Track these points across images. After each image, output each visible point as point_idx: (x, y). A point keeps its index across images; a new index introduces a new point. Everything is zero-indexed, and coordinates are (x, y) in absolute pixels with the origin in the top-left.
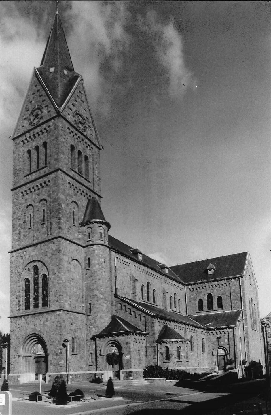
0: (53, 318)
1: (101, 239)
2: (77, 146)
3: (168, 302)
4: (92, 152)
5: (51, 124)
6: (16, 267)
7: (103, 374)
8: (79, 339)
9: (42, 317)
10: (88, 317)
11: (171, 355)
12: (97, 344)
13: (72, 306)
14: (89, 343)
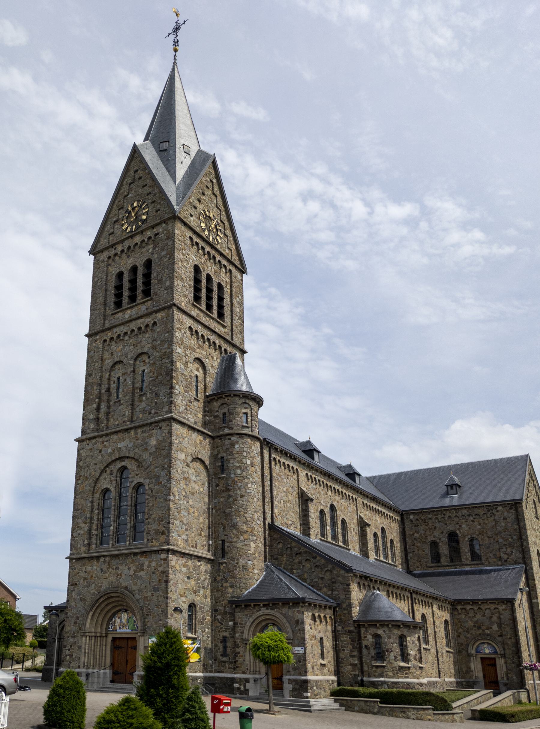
2: (206, 268)
5: (161, 230)
7: (249, 682)
9: (133, 561)
10: (219, 566)
14: (219, 617)
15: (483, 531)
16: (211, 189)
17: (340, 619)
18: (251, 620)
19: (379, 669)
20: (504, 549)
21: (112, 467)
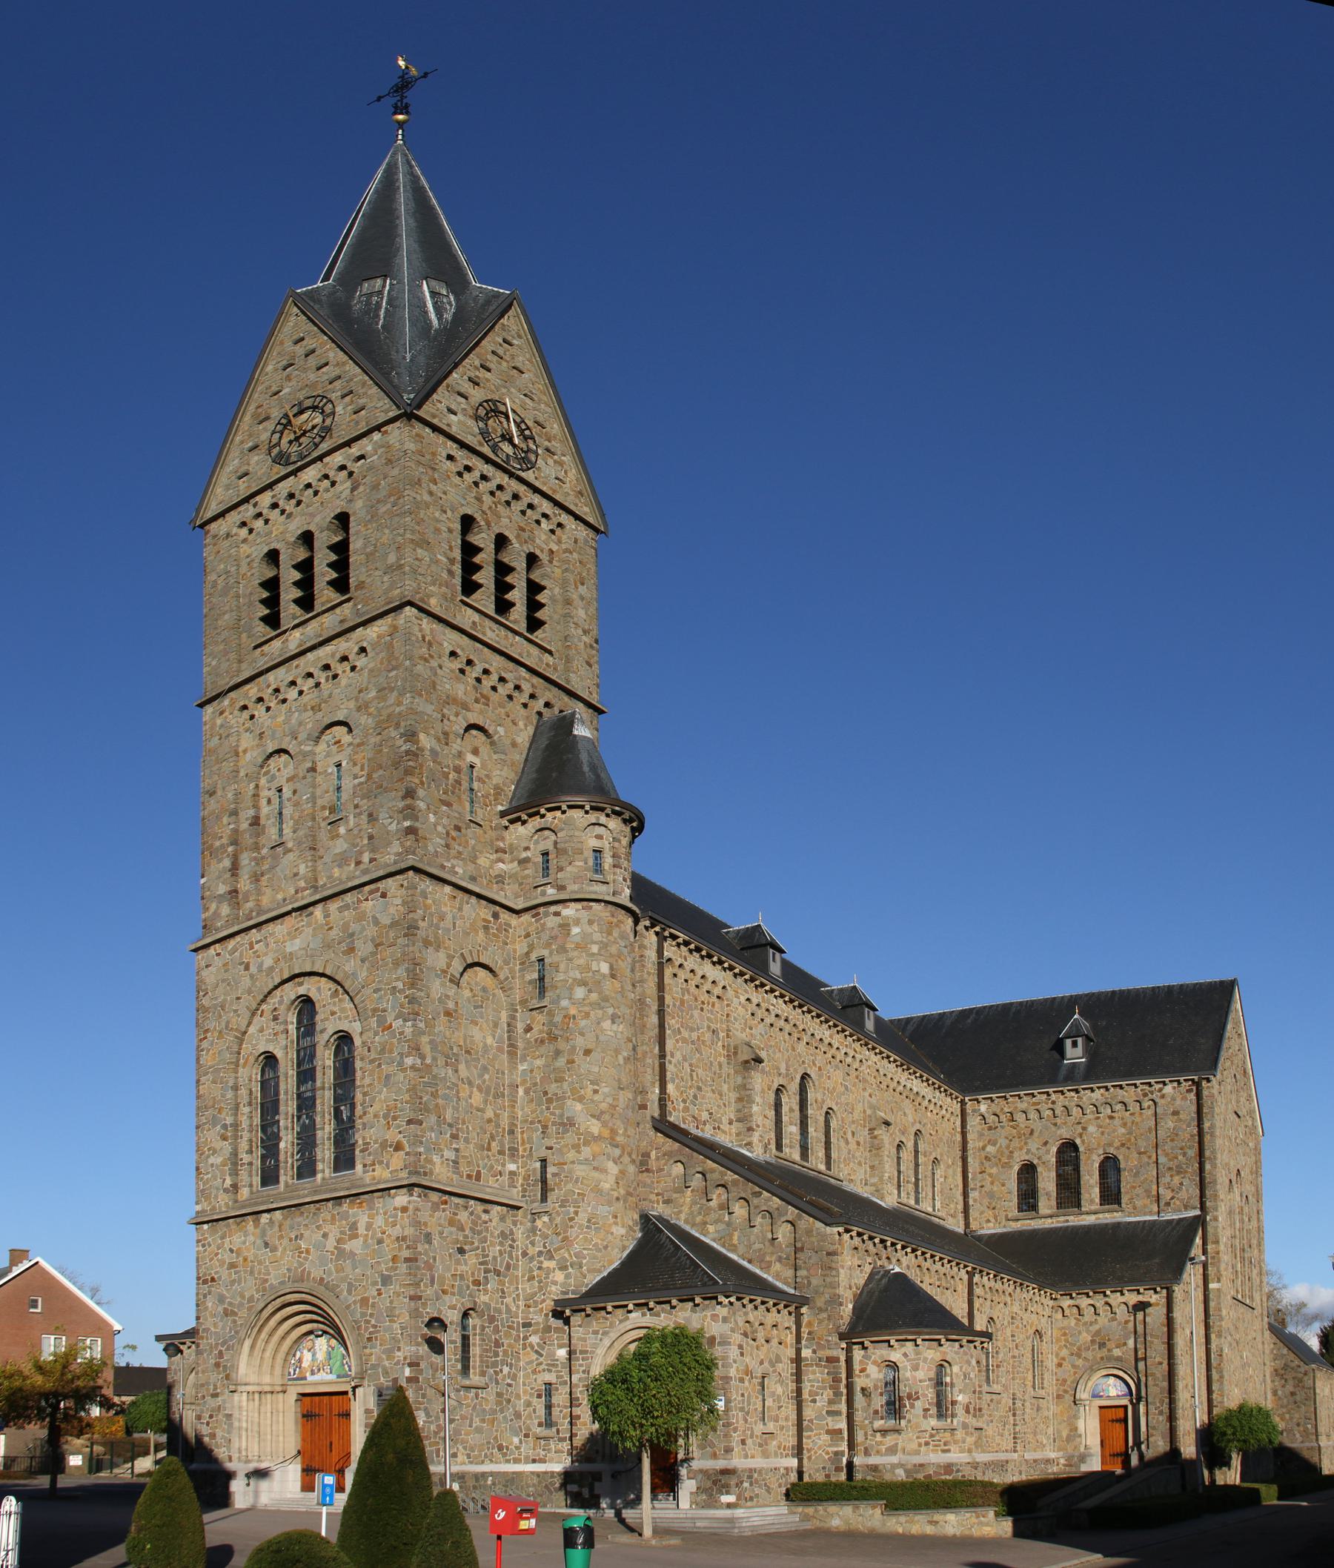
0: (379, 1221)
1: (597, 877)
3: (889, 1168)
6: (223, 1008)
10: (534, 1221)
13: (464, 1170)
15: (1129, 1140)
17: (809, 1333)
18: (607, 1342)
19: (888, 1438)
20: (1168, 1179)
21: (273, 1001)
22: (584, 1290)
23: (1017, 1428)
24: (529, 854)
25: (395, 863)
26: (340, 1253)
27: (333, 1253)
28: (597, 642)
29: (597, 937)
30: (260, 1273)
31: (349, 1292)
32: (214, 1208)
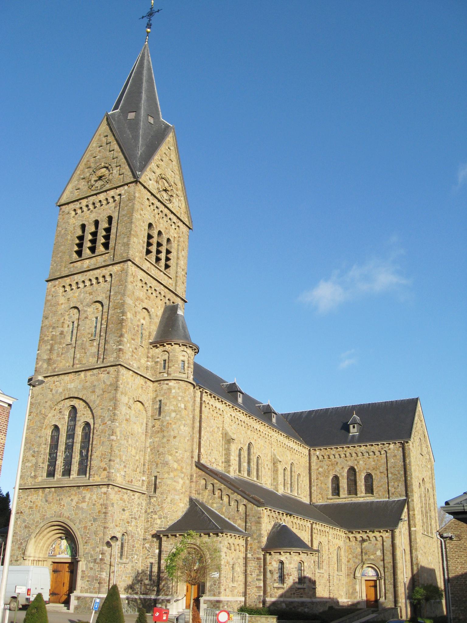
2: (157, 224)
3: (281, 479)
4: (178, 233)
8: (132, 537)
10: (150, 500)
11: (288, 575)
12: (163, 547)
13: (127, 479)
14: (147, 545)
16: (168, 155)
21: (60, 405)
22: (168, 527)
23: (331, 588)
24: (159, 360)
25: (114, 361)
26: (78, 507)
27: (74, 507)
28: (186, 274)
29: (181, 394)
30: (42, 512)
31: (80, 523)
32: (26, 484)
